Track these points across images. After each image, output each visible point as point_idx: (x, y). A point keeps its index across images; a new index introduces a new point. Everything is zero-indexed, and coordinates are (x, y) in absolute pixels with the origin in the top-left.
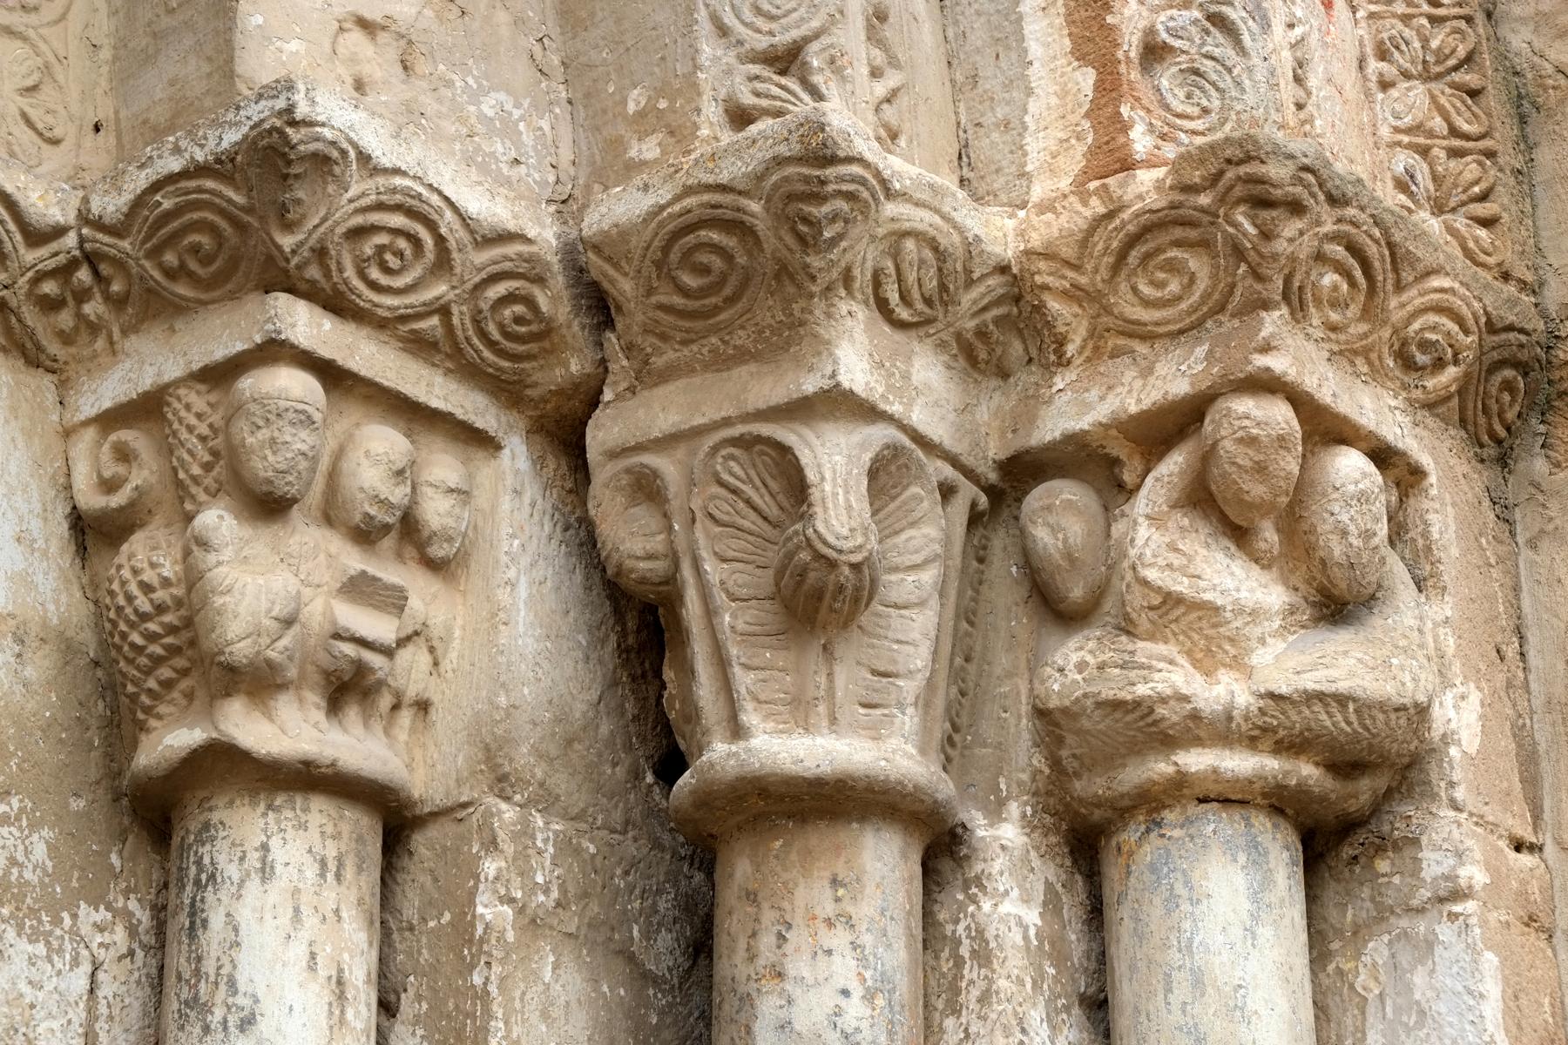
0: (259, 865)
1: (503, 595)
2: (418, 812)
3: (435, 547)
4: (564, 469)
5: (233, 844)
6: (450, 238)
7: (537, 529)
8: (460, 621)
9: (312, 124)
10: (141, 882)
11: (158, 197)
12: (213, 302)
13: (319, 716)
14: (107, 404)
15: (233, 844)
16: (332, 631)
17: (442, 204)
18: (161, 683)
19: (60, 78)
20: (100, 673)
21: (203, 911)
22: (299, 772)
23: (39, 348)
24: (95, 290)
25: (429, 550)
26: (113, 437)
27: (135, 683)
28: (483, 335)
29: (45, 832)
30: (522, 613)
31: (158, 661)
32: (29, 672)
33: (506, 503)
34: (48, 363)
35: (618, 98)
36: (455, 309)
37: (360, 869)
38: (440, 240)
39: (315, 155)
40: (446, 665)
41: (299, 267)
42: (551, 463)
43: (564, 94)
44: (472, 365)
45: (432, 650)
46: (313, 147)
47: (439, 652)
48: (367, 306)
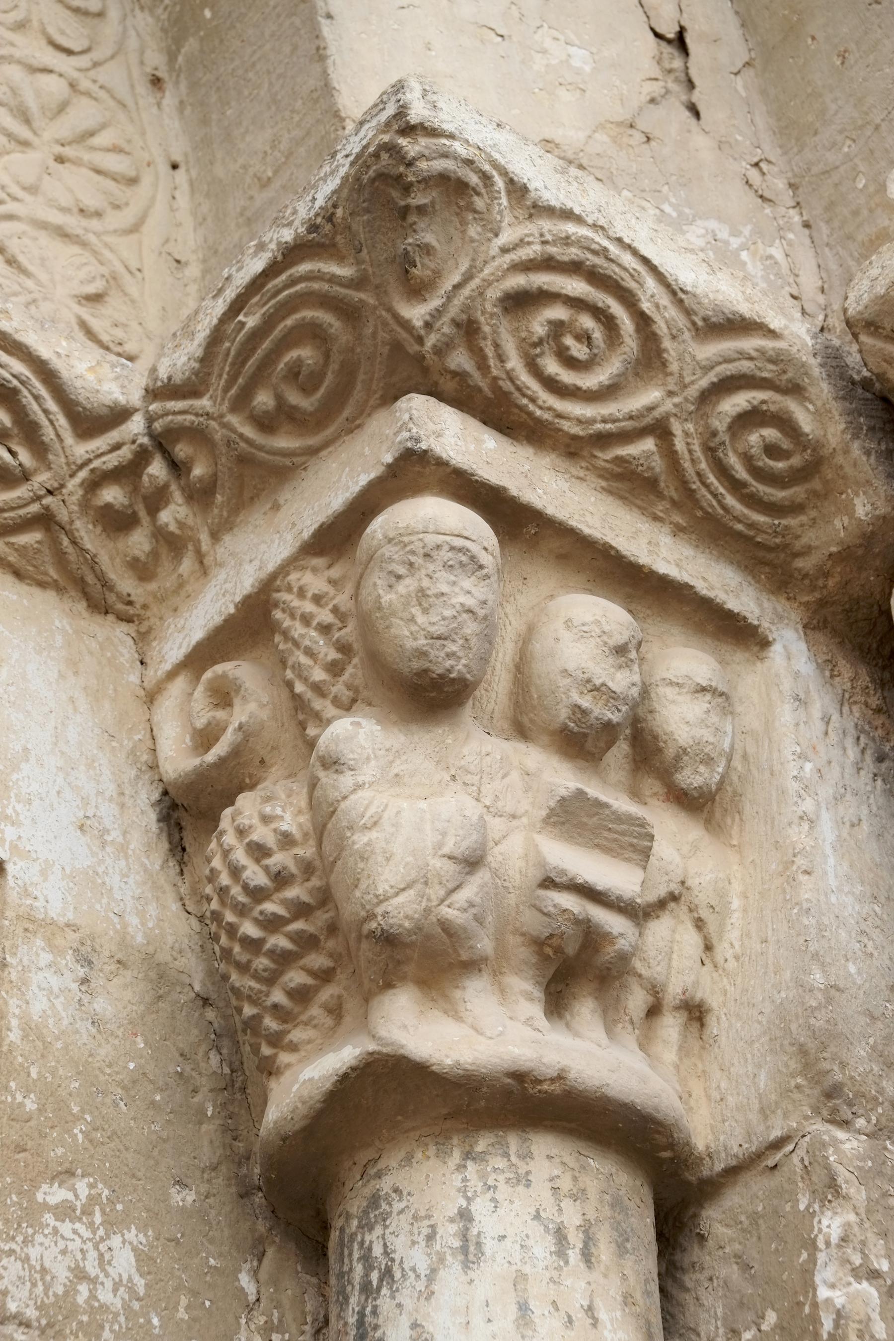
0: (457, 1243)
1: (798, 835)
2: (706, 1172)
3: (687, 772)
4: (865, 679)
5: (416, 1218)
6: (656, 317)
7: (836, 753)
8: (737, 887)
9: (433, 132)
10: (289, 1317)
11: (241, 318)
12: (326, 444)
13: (536, 1010)
14: (198, 636)
15: (416, 1218)
16: (540, 876)
17: (640, 267)
18: (291, 994)
19: (133, 290)
20: (210, 1014)
21: (376, 1327)
22: (507, 1093)
23: (106, 584)
24: (173, 487)
25: (678, 777)
26: (208, 674)
27: (254, 1002)
28: (723, 471)
29: (132, 1235)
30: (831, 861)
31: (284, 959)
32: (101, 1005)
33: (786, 714)
34: (120, 606)
35: (872, 189)
36: (676, 427)
37: (621, 1250)
38: (643, 321)
39: (443, 178)
40: (723, 950)
41: (440, 351)
42: (846, 670)
43: (797, 219)
44: (709, 517)
45: (699, 924)
46: (439, 165)
47: (712, 927)
48: (547, 416)
